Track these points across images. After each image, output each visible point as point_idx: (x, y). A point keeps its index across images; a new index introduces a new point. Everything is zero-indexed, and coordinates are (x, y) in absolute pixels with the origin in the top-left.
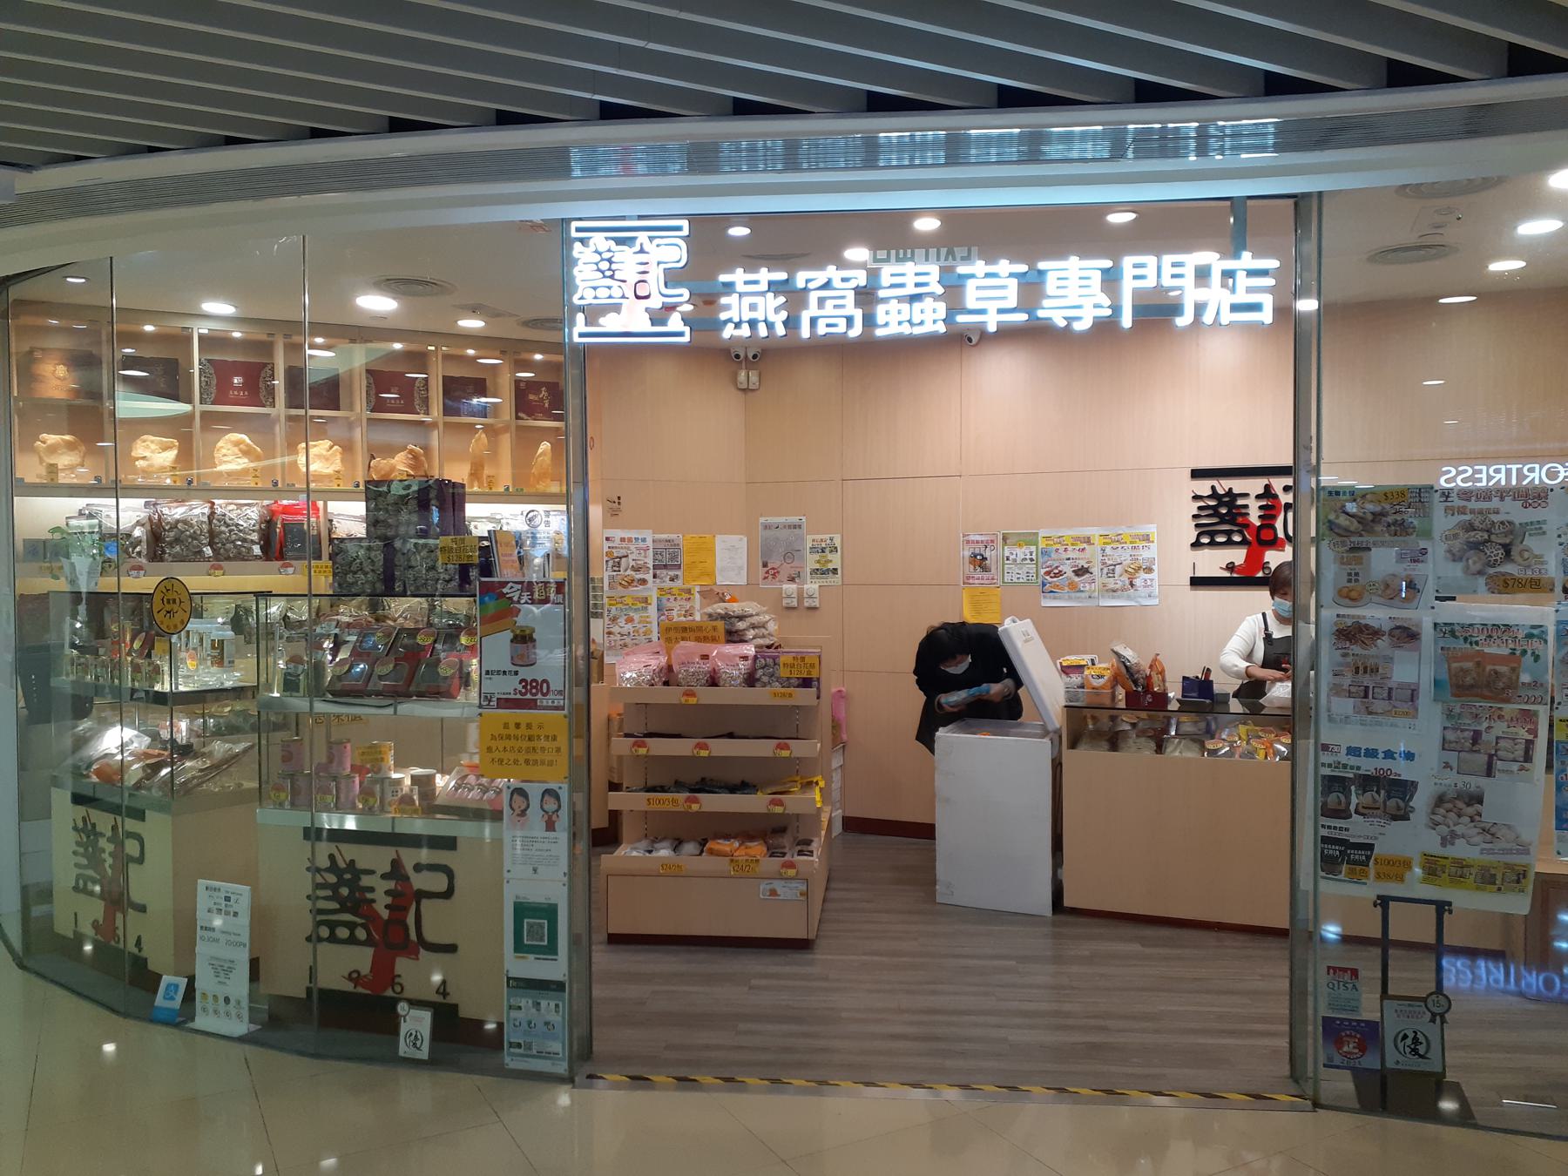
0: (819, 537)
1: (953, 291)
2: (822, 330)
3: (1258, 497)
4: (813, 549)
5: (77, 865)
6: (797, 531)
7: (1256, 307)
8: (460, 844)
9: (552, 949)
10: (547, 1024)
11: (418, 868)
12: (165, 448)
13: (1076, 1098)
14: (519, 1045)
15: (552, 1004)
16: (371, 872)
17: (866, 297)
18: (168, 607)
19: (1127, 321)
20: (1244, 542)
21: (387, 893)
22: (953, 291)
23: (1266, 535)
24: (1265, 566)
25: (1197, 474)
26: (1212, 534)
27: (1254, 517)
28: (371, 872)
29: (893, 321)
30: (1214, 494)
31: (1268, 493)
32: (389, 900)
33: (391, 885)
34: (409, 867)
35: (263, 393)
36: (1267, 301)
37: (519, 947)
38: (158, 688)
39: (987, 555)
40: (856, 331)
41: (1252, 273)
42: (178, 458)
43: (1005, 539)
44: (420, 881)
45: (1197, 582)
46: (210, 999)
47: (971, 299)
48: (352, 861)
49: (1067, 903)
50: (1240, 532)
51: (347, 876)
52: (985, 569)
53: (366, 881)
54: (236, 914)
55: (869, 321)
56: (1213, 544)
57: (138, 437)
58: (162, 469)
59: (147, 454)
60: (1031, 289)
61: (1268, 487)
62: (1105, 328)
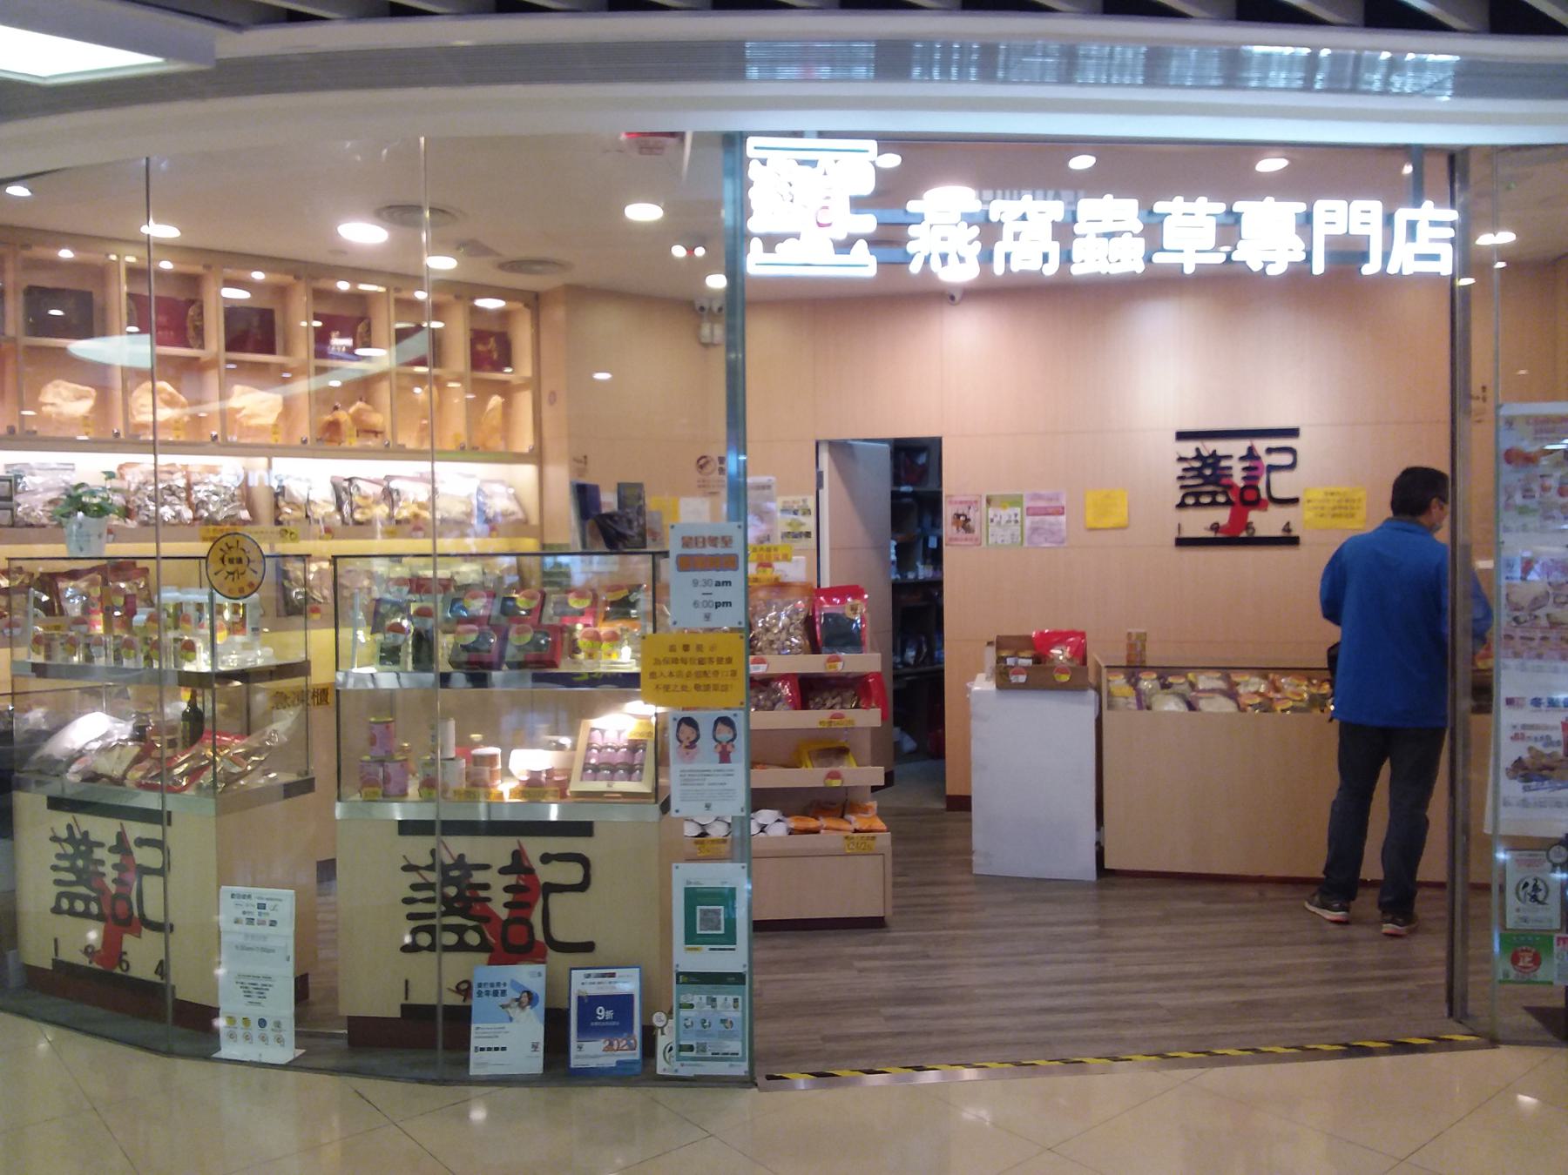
0: (790, 498)
1: (1152, 230)
2: (1016, 267)
3: (1242, 459)
4: (784, 510)
5: (58, 882)
6: (766, 492)
7: (1435, 257)
8: (597, 829)
9: (730, 937)
10: (723, 1021)
11: (546, 858)
12: (80, 397)
13: (1179, 1063)
14: (691, 1048)
15: (730, 999)
16: (486, 867)
17: (1064, 232)
18: (230, 568)
19: (1318, 267)
20: (1228, 503)
21: (507, 889)
22: (1152, 230)
23: (1250, 496)
24: (1248, 526)
25: (1182, 436)
26: (1197, 495)
27: (1238, 478)
28: (486, 867)
29: (1091, 259)
30: (1199, 457)
31: (1251, 454)
32: (508, 897)
33: (511, 880)
34: (533, 857)
35: (191, 333)
36: (1447, 252)
37: (691, 938)
38: (188, 667)
39: (971, 515)
40: (1051, 269)
41: (1434, 224)
42: (94, 409)
43: (989, 501)
44: (548, 874)
45: (1182, 542)
46: (240, 1023)
47: (1170, 237)
48: (461, 856)
49: (1107, 866)
50: (1225, 493)
51: (455, 873)
52: (968, 530)
53: (478, 877)
54: (273, 923)
55: (1067, 258)
56: (1198, 504)
57: (50, 380)
58: (72, 421)
59: (58, 401)
60: (1230, 228)
61: (1251, 449)
62: (1298, 275)
